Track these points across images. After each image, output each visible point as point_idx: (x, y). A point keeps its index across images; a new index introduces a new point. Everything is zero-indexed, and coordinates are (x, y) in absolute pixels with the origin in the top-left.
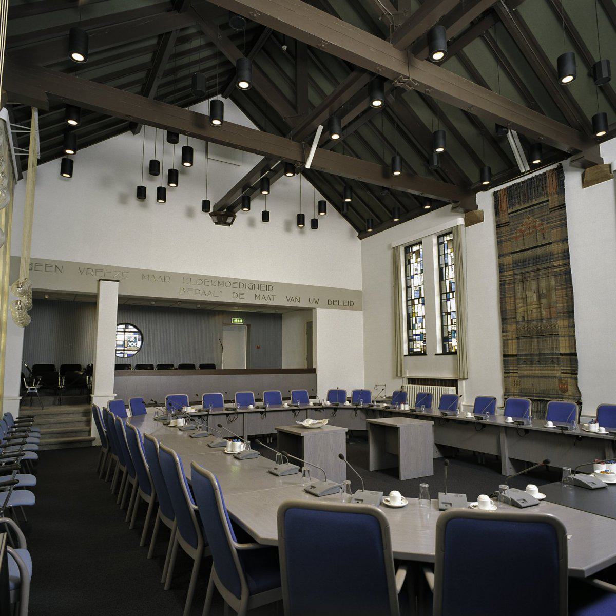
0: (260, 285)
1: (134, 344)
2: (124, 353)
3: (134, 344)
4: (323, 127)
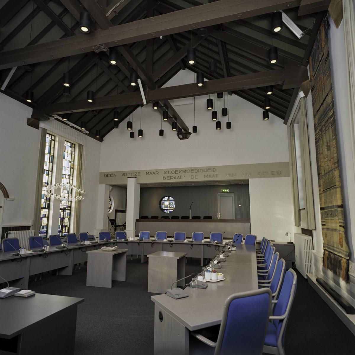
0: (208, 169)
1: (172, 206)
2: (168, 211)
3: (172, 206)
4: (302, 92)
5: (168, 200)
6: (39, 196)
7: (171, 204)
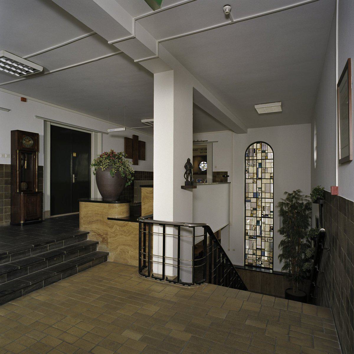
5: (204, 163)
6: (245, 168)
7: (205, 166)
